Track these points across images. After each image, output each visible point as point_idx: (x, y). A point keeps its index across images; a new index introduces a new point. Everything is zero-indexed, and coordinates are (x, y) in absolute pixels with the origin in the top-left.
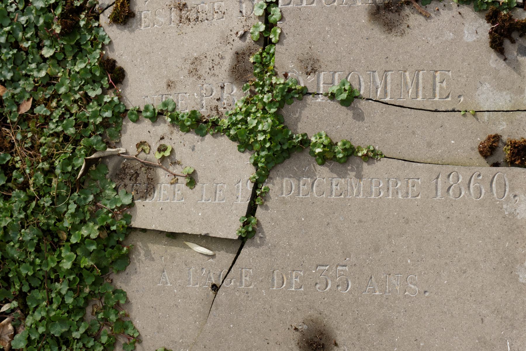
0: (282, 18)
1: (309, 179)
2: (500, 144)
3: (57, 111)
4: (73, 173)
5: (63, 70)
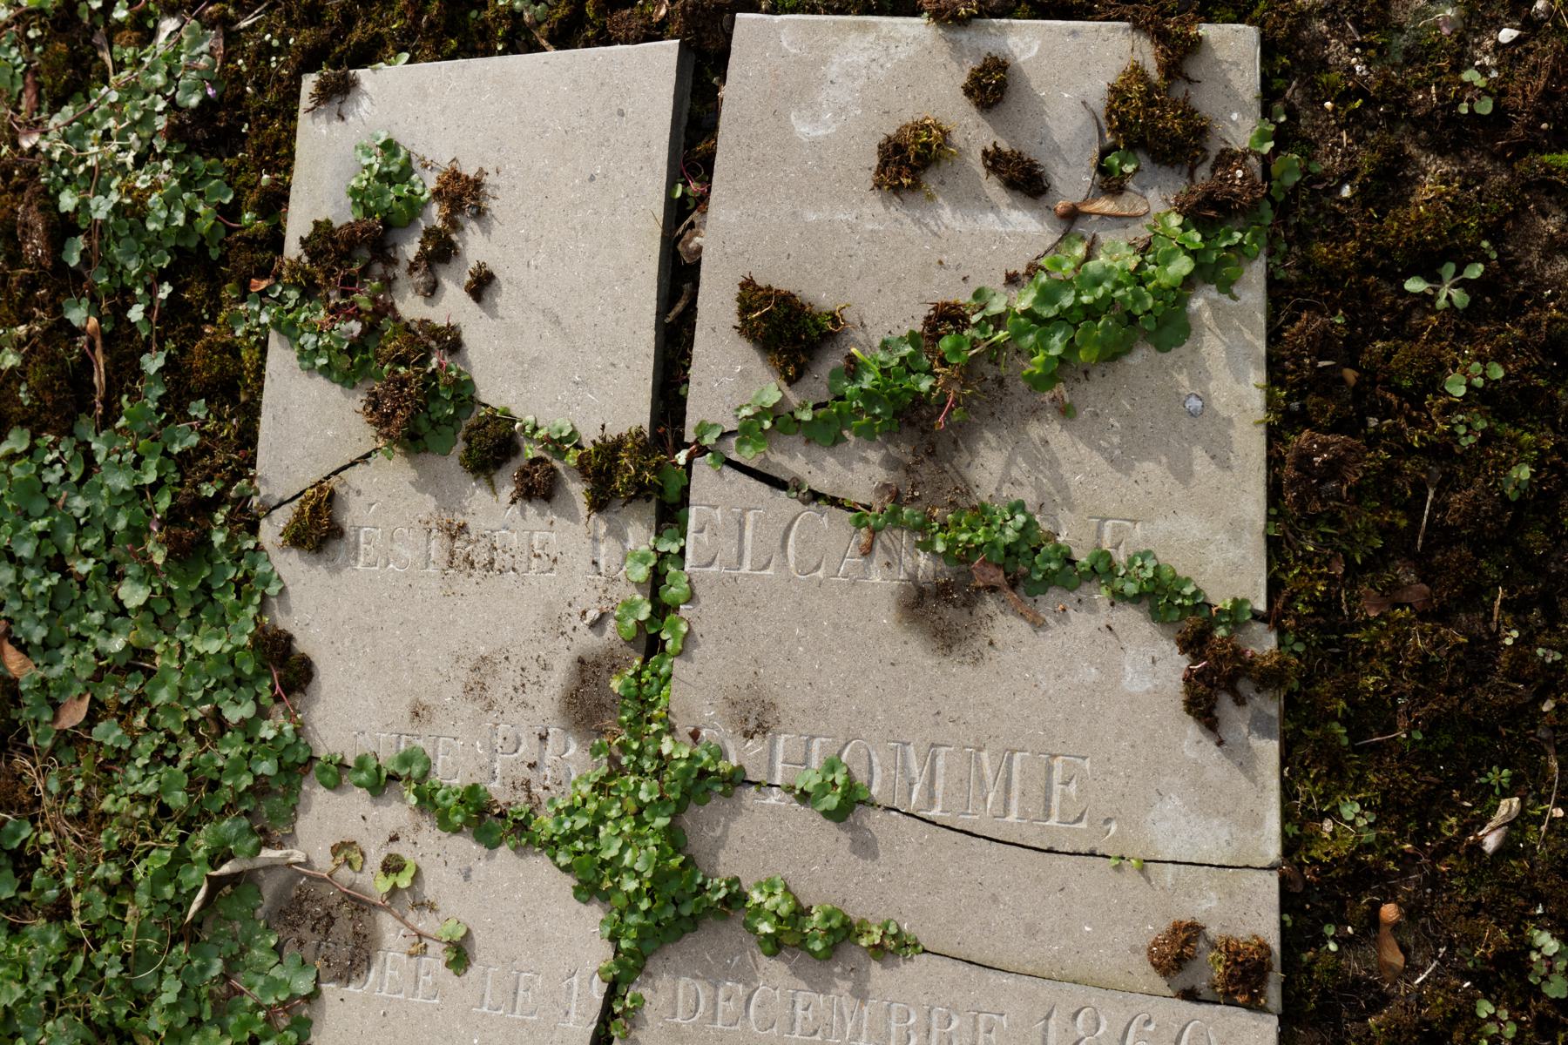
0: (691, 598)
1: (741, 986)
2: (1202, 944)
3: (147, 740)
4: (176, 902)
5: (166, 640)
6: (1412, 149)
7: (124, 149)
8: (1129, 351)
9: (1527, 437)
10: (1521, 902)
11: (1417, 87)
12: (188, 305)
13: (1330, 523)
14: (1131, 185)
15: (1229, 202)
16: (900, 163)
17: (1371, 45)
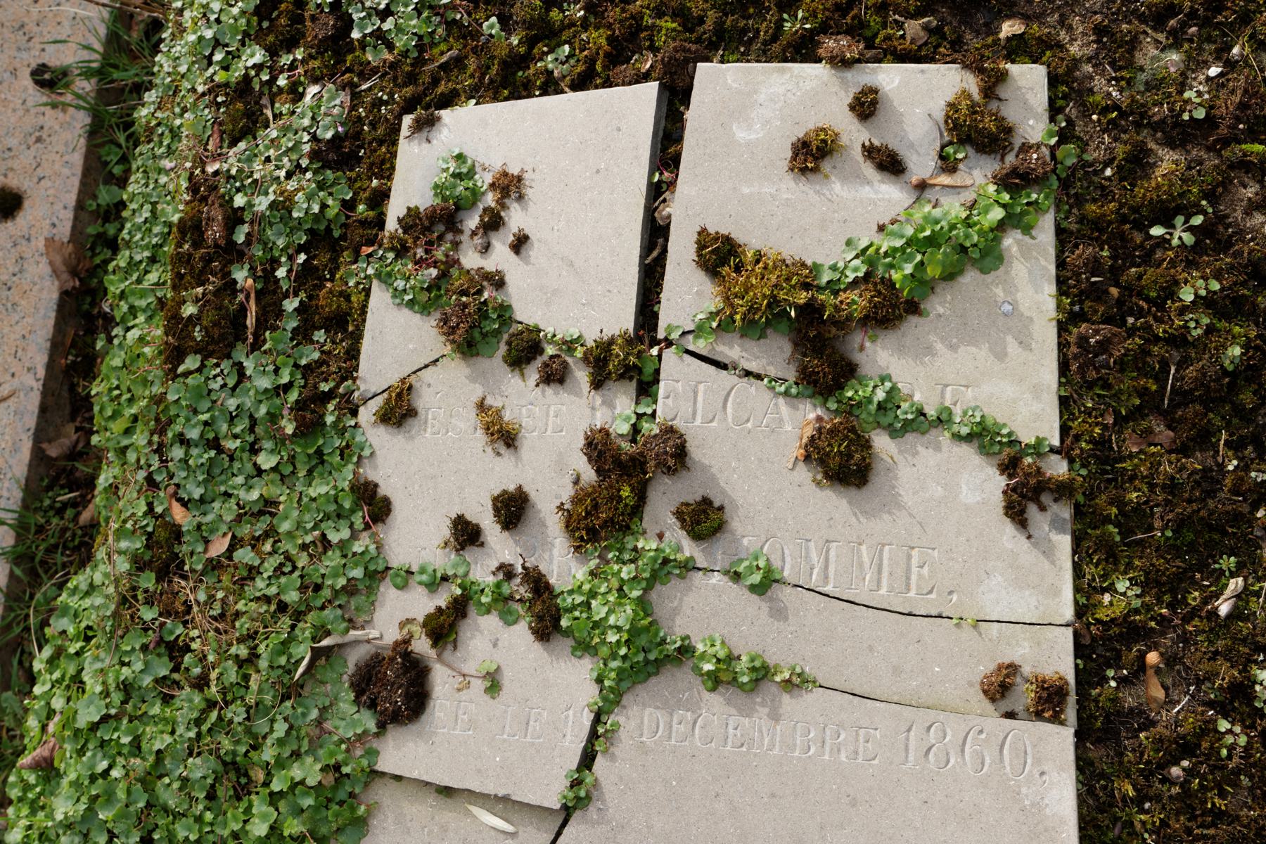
2: (1018, 680)
3: (271, 560)
6: (1152, 145)
7: (278, 168)
8: (961, 272)
9: (1237, 329)
10: (1247, 650)
11: (1155, 105)
12: (316, 268)
13: (1103, 388)
14: (961, 166)
15: (1028, 173)
16: (807, 154)
17: (1122, 78)
